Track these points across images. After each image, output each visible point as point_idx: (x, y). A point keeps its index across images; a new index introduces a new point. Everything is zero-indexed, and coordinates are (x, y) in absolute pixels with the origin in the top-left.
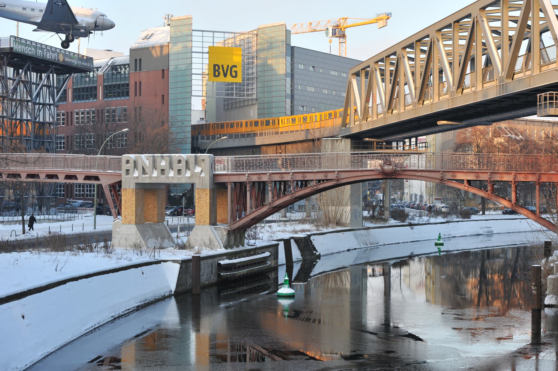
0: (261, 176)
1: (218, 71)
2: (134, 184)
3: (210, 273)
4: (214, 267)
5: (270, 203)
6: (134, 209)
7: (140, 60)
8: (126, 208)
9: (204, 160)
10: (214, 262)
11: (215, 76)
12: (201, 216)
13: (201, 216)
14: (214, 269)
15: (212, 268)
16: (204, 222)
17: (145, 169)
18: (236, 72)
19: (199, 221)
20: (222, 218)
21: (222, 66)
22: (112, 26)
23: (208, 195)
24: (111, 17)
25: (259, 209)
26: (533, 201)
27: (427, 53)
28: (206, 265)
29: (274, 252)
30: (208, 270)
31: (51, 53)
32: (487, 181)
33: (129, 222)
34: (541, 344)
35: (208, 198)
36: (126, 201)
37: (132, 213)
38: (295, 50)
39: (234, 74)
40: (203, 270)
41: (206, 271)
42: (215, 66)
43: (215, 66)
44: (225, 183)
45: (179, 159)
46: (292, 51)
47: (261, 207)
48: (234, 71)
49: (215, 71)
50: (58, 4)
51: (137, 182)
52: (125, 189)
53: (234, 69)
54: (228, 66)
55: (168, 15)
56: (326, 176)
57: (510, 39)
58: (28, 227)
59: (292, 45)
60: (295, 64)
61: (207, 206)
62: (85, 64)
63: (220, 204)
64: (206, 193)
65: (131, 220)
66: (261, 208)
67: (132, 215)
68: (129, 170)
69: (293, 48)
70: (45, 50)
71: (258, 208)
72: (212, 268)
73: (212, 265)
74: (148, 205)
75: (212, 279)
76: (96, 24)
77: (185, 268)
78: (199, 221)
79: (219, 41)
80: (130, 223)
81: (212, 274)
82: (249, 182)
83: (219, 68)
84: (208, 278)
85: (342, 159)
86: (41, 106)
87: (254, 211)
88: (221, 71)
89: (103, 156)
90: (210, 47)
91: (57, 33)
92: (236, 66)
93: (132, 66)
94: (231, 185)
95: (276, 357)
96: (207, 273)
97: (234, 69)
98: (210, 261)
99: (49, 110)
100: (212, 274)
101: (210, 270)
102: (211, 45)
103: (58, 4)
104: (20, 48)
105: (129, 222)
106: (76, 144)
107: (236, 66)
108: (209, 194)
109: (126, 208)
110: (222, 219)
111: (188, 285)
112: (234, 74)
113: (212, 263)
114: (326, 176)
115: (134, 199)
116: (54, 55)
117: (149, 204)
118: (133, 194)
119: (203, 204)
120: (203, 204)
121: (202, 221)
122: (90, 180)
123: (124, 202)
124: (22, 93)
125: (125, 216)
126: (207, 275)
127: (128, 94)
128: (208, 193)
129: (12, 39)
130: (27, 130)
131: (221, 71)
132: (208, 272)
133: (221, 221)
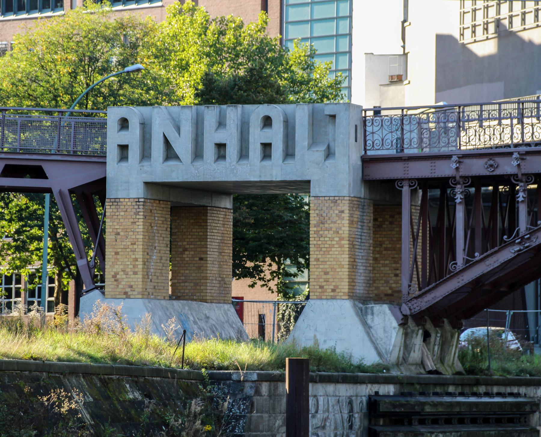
2: (141, 186)
3: (346, 425)
4: (356, 408)
5: (522, 238)
6: (139, 255)
8: (117, 253)
9: (333, 117)
10: (357, 396)
12: (326, 273)
13: (326, 273)
14: (356, 416)
15: (351, 410)
16: (333, 290)
17: (173, 145)
19: (321, 287)
20: (391, 288)
25: (492, 254)
28: (332, 401)
30: (338, 416)
33: (126, 293)
36: (118, 234)
37: (135, 266)
40: (324, 412)
41: (331, 416)
45: (267, 114)
47: (496, 248)
51: (150, 181)
52: (116, 201)
63: (386, 249)
64: (339, 208)
65: (131, 287)
66: (496, 252)
67: (135, 273)
71: (489, 252)
72: (351, 410)
73: (350, 403)
74: (182, 253)
77: (270, 396)
78: (321, 287)
80: (127, 296)
81: (351, 427)
82: (464, 178)
87: (477, 259)
89: (259, 414)
94: (410, 186)
95: (405, 403)
96: (336, 423)
100: (351, 427)
101: (346, 416)
106: (205, 387)
110: (390, 292)
113: (350, 398)
115: (140, 227)
117: (185, 250)
118: (137, 213)
119: (332, 239)
120: (332, 239)
121: (329, 288)
123: (113, 237)
125: (114, 276)
126: (336, 428)
132: (339, 421)
133: (387, 295)
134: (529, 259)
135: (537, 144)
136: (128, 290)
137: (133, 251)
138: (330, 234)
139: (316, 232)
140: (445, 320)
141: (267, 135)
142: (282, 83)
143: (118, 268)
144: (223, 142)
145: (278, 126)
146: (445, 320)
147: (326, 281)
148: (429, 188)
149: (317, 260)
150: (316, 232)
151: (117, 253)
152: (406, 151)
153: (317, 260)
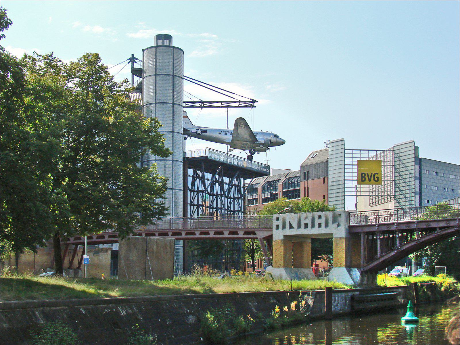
4: (347, 298)
6: (283, 256)
7: (308, 172)
8: (276, 255)
11: (362, 180)
16: (340, 265)
18: (378, 178)
21: (368, 174)
22: (283, 143)
23: (344, 243)
24: (282, 136)
29: (403, 293)
31: (237, 161)
33: (279, 266)
35: (344, 245)
37: (281, 259)
38: (422, 160)
39: (376, 179)
41: (339, 302)
43: (362, 174)
44: (358, 233)
46: (419, 161)
48: (376, 177)
49: (362, 177)
50: (242, 126)
53: (376, 176)
54: (372, 173)
55: (328, 141)
59: (420, 157)
60: (422, 170)
62: (263, 170)
67: (281, 261)
69: (420, 159)
70: (233, 159)
75: (346, 309)
76: (271, 141)
79: (365, 157)
80: (279, 267)
83: (365, 175)
84: (342, 308)
86: (232, 200)
88: (366, 177)
90: (358, 161)
91: (244, 150)
92: (377, 174)
93: (303, 177)
97: (376, 176)
98: (344, 295)
99: (238, 203)
101: (344, 302)
102: (359, 159)
103: (242, 126)
104: (213, 156)
107: (377, 174)
108: (344, 242)
109: (276, 255)
111: (323, 313)
112: (376, 179)
114: (449, 224)
116: (239, 162)
120: (340, 250)
121: (339, 264)
122: (250, 235)
124: (216, 189)
125: (275, 262)
127: (299, 197)
128: (344, 241)
129: (207, 150)
130: (202, 199)
131: (366, 177)
143: (276, 259)
145: (323, 218)
148: (183, 242)
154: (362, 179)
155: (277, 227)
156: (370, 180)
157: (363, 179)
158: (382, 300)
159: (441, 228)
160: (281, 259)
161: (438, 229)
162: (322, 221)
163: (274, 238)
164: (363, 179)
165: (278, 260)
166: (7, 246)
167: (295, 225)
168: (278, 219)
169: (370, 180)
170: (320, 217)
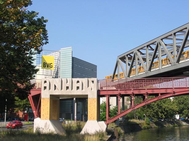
0: (141, 90)
1: (45, 65)
11: (44, 67)
16: (93, 118)
18: (52, 66)
26: (126, 98)
27: (154, 50)
32: (118, 95)
33: (46, 119)
34: (142, 129)
37: (48, 113)
38: (74, 58)
39: (51, 66)
42: (44, 63)
43: (44, 63)
53: (51, 65)
54: (49, 64)
56: (167, 91)
57: (178, 47)
58: (32, 11)
61: (95, 109)
67: (48, 114)
68: (79, 87)
80: (46, 119)
85: (118, 87)
92: (52, 64)
105: (46, 119)
107: (52, 64)
121: (92, 118)
125: (43, 115)
134: (184, 73)
135: (188, 88)
136: (46, 118)
137: (47, 109)
138: (93, 106)
139: (90, 106)
140: (129, 120)
141: (78, 85)
142: (31, 69)
143: (43, 113)
144: (78, 86)
145: (80, 83)
146: (129, 120)
147: (92, 116)
148: (101, 97)
149: (90, 112)
150: (90, 106)
151: (44, 110)
152: (187, 86)
153: (90, 112)
154: (44, 66)
155: (45, 88)
156: (48, 67)
157: (45, 66)
158: (3, 128)
159: (162, 94)
160: (48, 113)
161: (160, 94)
162: (80, 85)
163: (43, 96)
164: (45, 66)
165: (45, 114)
166: (24, 86)
167: (58, 86)
168: (78, 82)
169: (48, 67)
170: (78, 82)
